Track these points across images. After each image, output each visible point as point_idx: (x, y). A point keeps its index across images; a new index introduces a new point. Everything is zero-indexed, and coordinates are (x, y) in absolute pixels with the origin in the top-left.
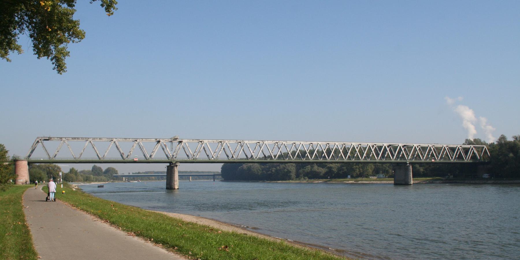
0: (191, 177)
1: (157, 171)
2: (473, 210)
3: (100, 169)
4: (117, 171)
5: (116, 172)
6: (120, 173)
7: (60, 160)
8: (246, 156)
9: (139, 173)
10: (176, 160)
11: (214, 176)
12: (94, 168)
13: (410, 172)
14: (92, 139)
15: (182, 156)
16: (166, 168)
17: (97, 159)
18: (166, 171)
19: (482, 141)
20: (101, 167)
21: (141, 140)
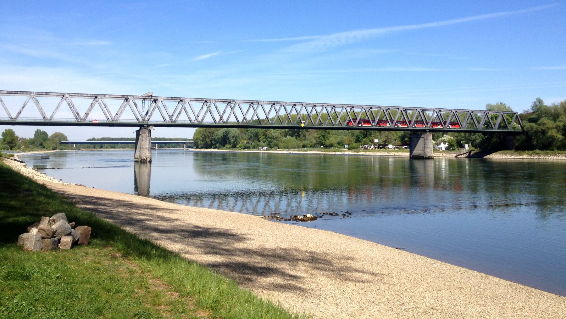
0: (157, 145)
1: (120, 137)
2: (418, 316)
3: (45, 133)
4: (66, 137)
5: (65, 138)
6: (70, 139)
7: (24, 120)
8: (237, 119)
9: (94, 139)
10: (149, 122)
11: (40, 159)
12: (38, 133)
13: (502, 130)
14: (35, 93)
15: (156, 118)
16: (135, 133)
17: (41, 119)
18: (135, 137)
19: (273, 117)
20: (46, 131)
21: (103, 96)
